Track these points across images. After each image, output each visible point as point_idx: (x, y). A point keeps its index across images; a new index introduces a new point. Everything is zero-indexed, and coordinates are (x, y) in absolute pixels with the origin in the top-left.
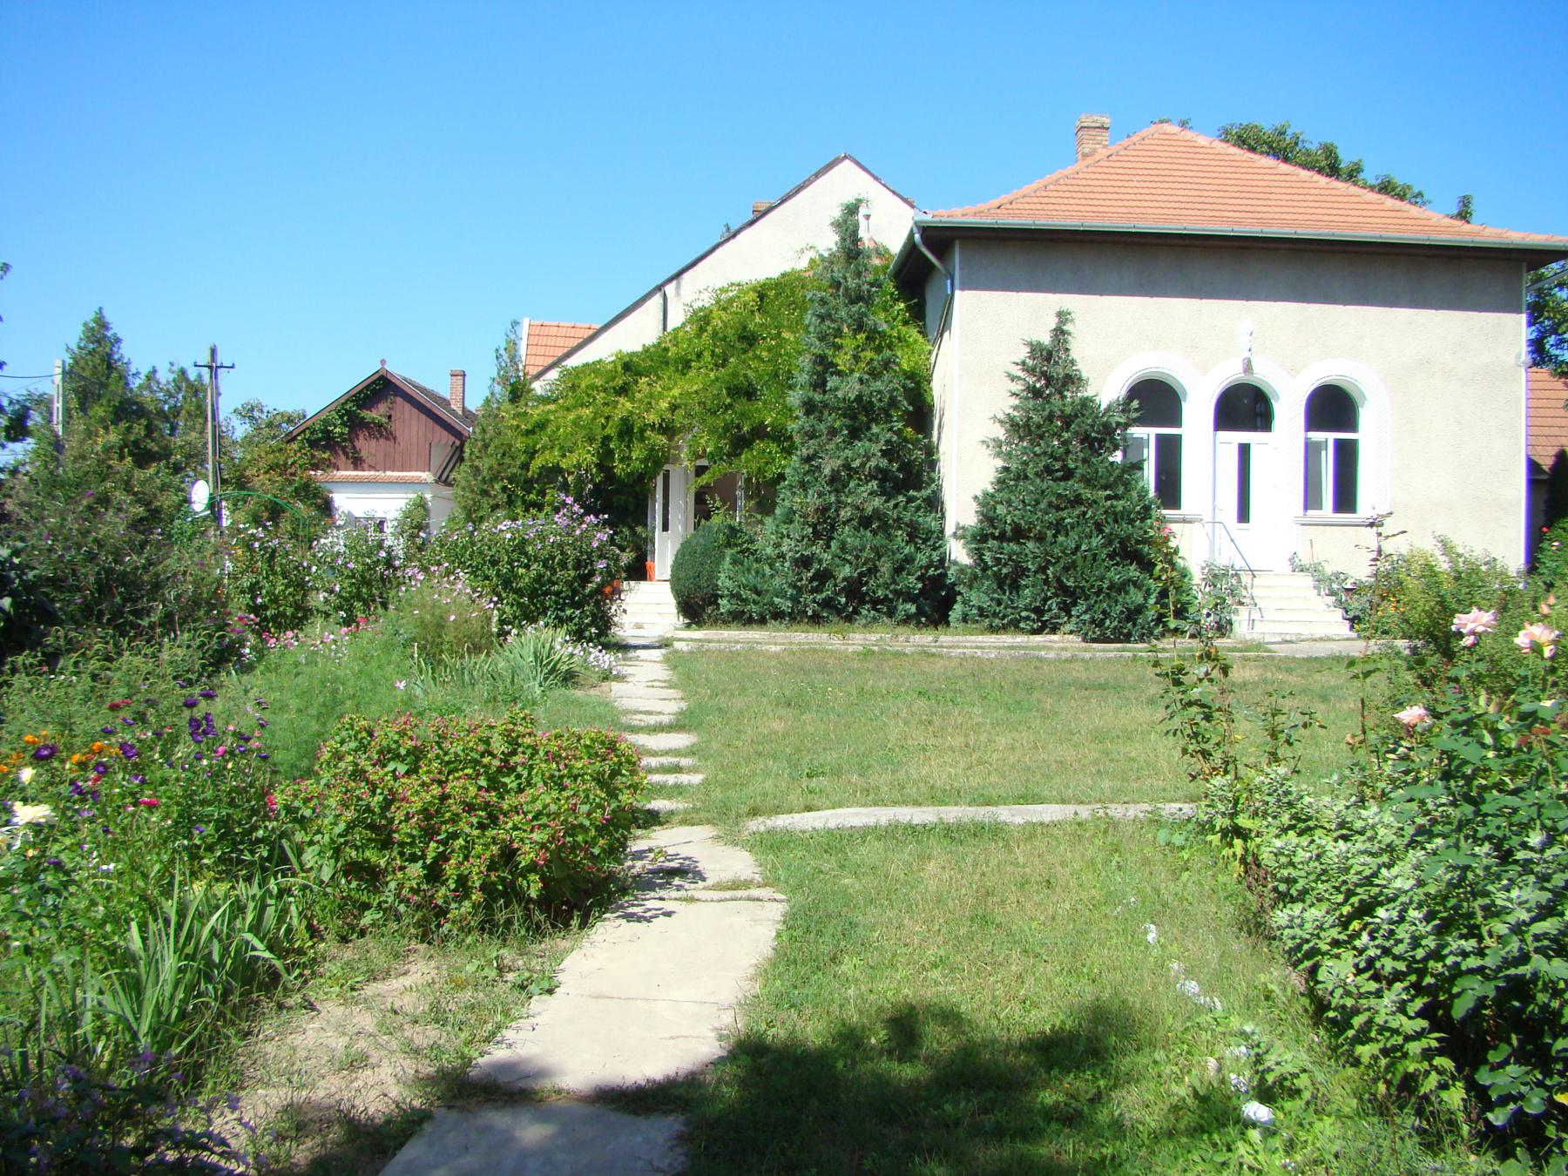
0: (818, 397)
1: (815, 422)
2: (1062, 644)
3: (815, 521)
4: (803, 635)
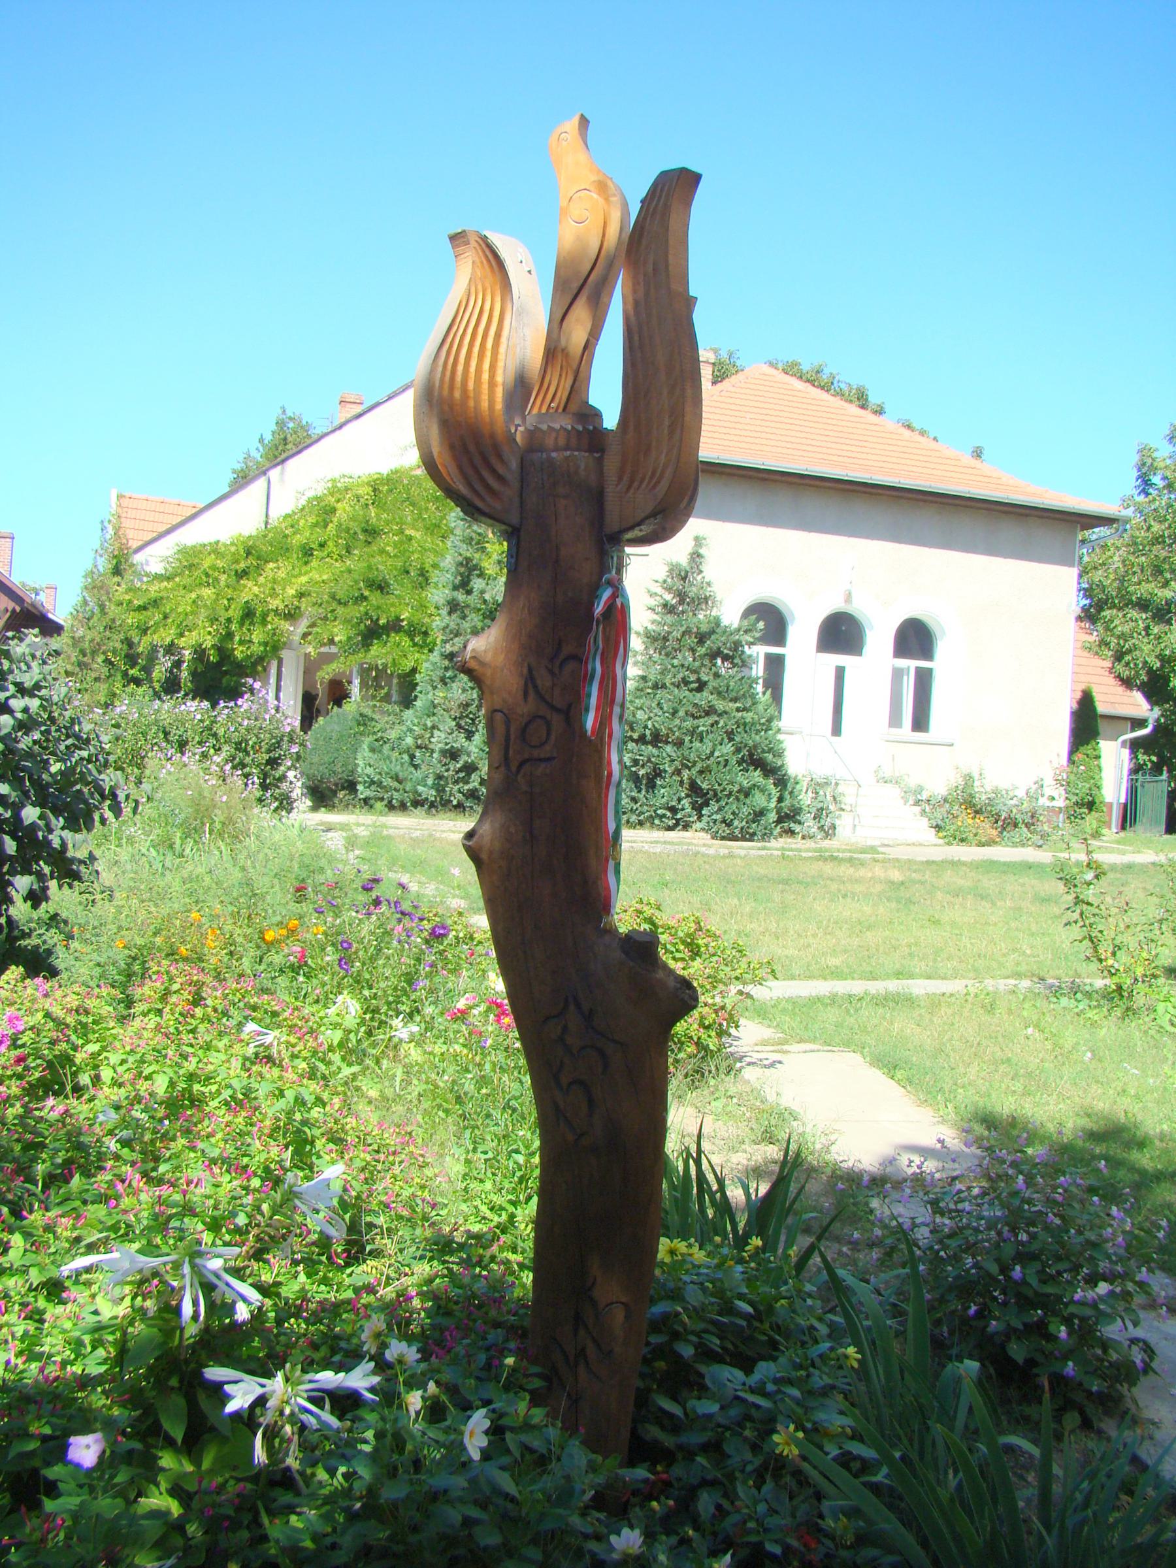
0: (460, 596)
1: (459, 621)
2: (697, 839)
3: (458, 715)
4: (452, 823)
